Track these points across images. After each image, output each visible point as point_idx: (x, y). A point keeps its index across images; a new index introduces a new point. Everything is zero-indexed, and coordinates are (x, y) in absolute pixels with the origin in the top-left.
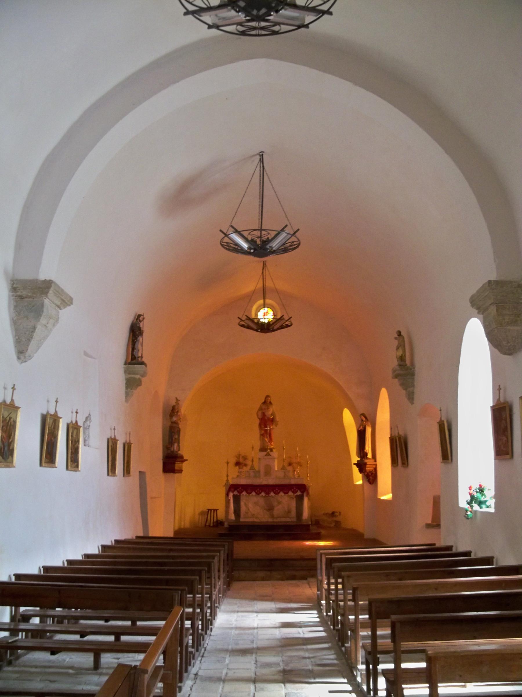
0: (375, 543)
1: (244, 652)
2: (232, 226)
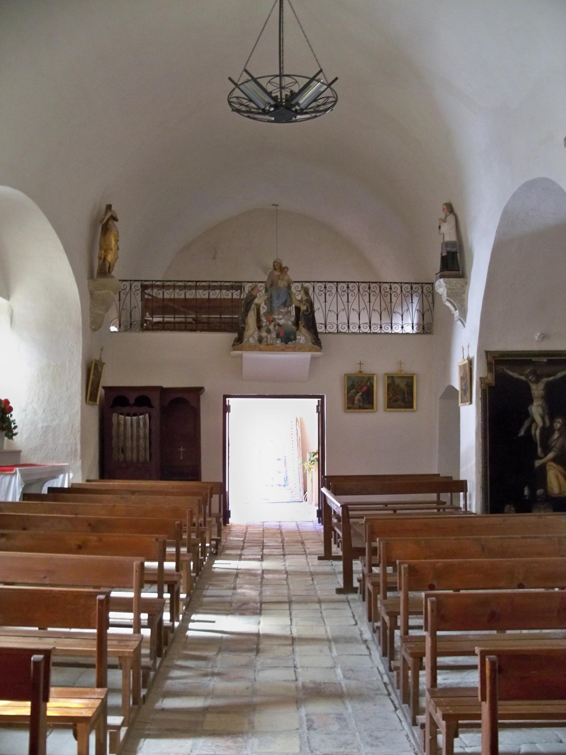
0: (470, 362)
1: (317, 692)
2: (246, 71)
